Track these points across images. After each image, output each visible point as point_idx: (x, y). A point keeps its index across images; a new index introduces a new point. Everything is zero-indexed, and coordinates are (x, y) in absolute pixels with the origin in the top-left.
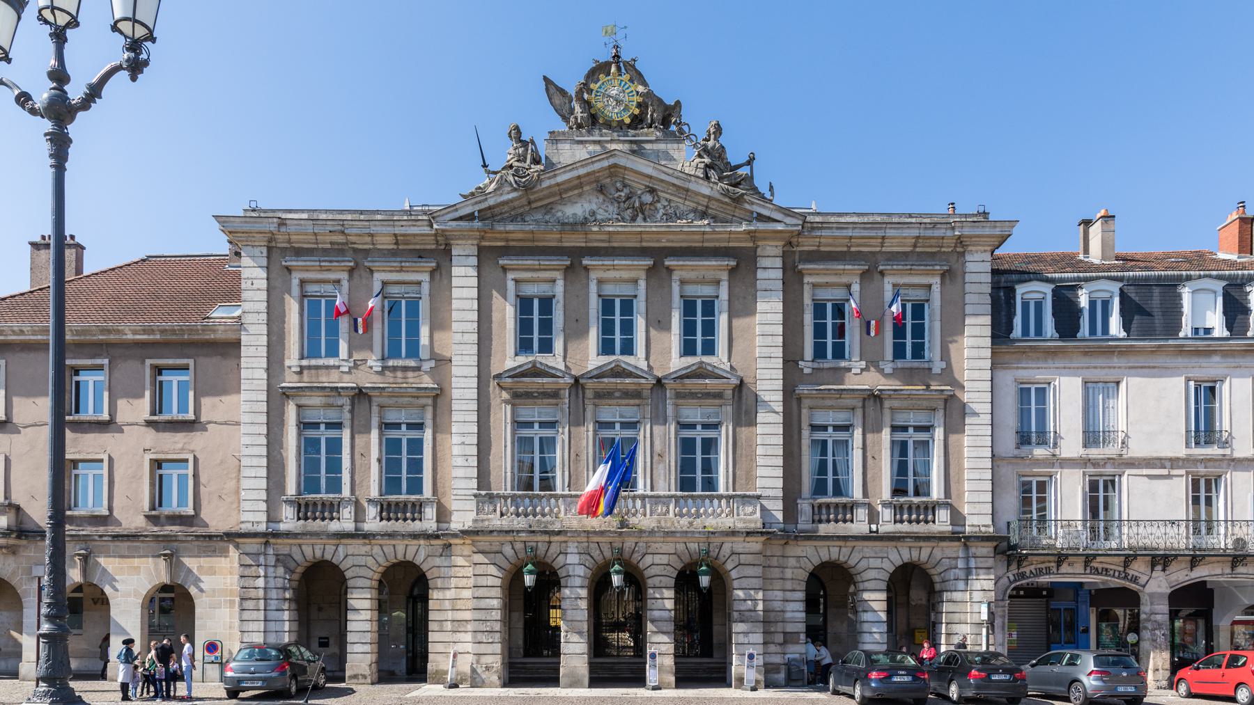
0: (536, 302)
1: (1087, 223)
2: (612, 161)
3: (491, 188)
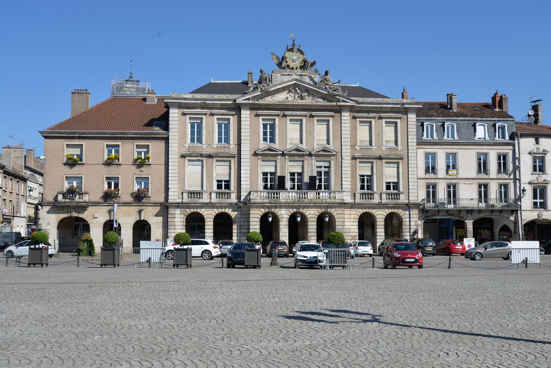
0: (268, 126)
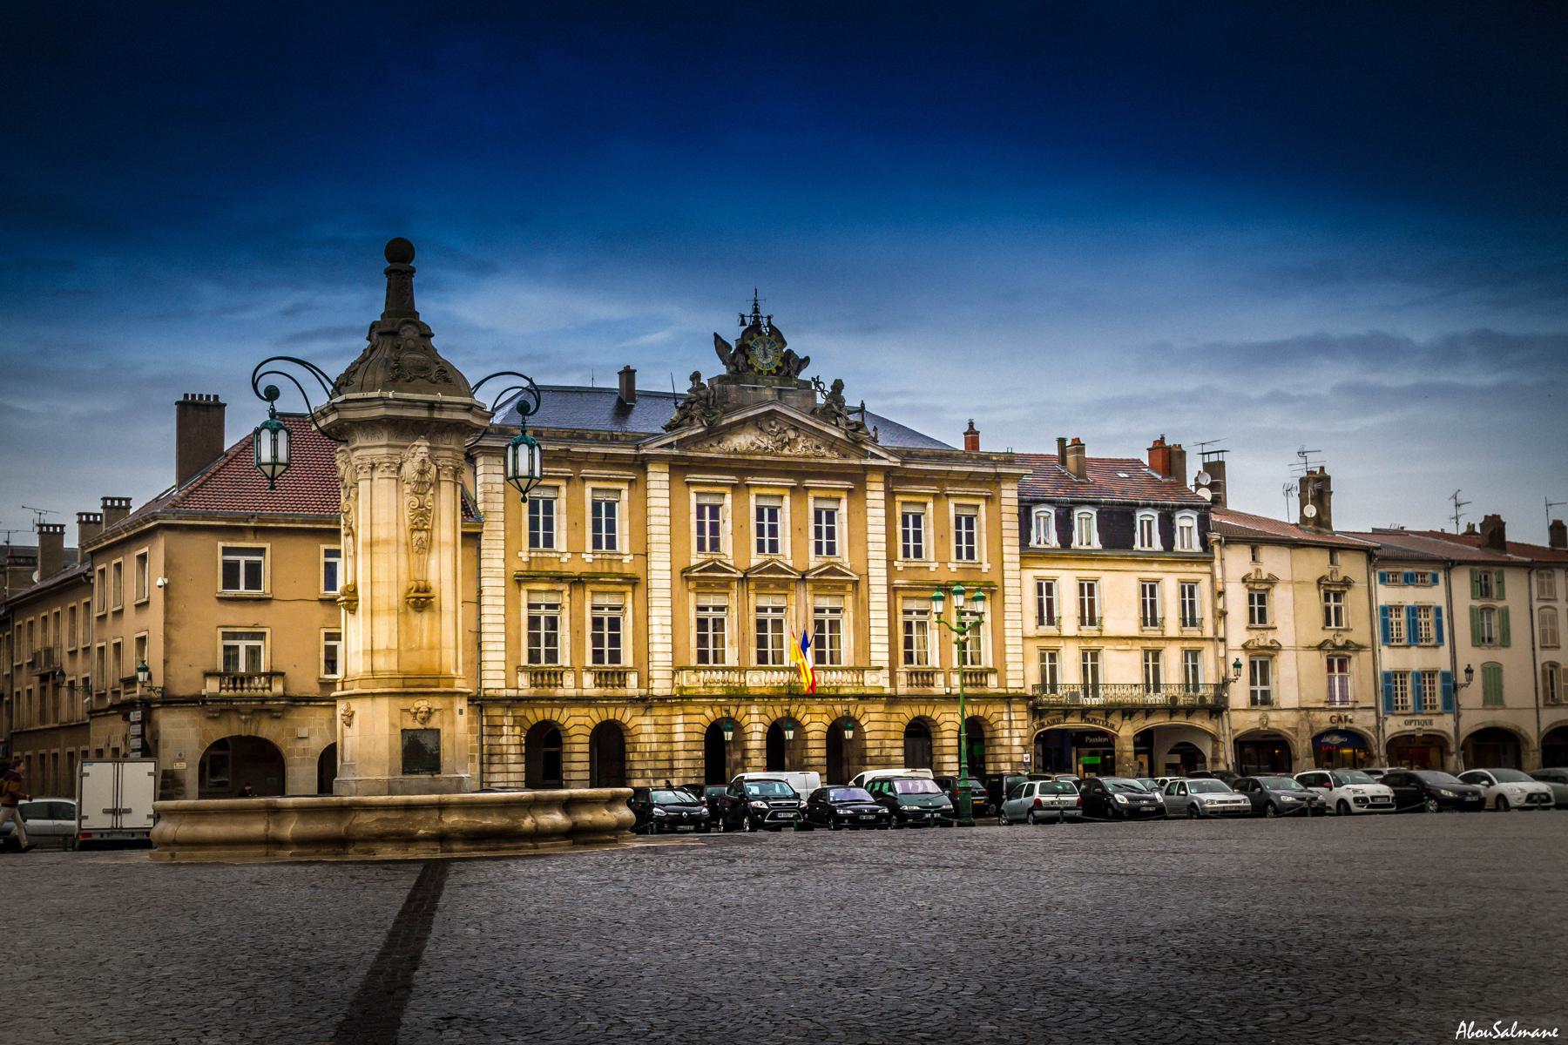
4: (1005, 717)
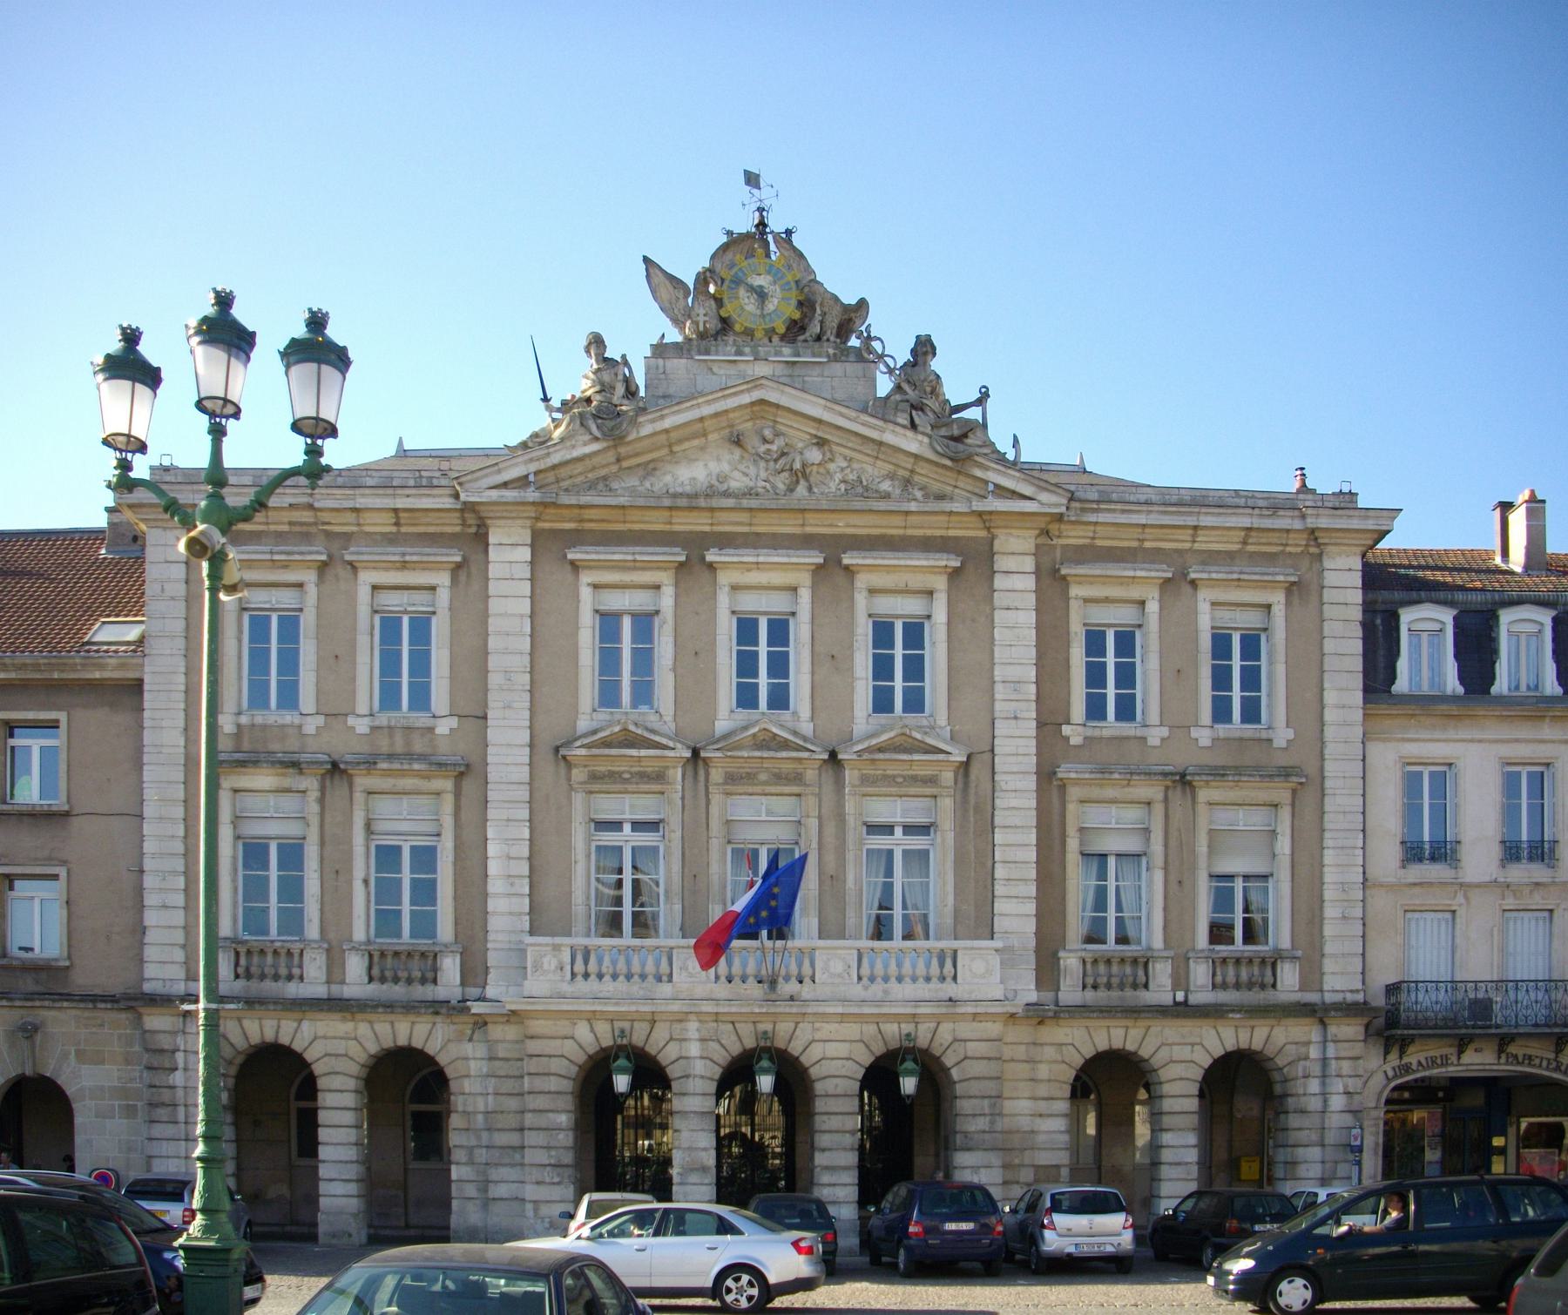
0: (627, 623)
1: (1506, 507)
2: (757, 395)
3: (557, 434)
4: (1314, 1053)
